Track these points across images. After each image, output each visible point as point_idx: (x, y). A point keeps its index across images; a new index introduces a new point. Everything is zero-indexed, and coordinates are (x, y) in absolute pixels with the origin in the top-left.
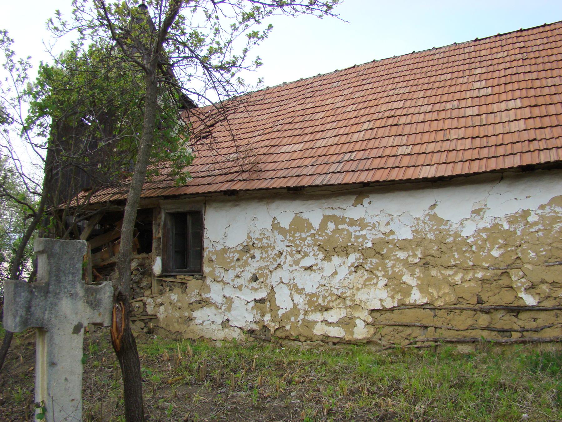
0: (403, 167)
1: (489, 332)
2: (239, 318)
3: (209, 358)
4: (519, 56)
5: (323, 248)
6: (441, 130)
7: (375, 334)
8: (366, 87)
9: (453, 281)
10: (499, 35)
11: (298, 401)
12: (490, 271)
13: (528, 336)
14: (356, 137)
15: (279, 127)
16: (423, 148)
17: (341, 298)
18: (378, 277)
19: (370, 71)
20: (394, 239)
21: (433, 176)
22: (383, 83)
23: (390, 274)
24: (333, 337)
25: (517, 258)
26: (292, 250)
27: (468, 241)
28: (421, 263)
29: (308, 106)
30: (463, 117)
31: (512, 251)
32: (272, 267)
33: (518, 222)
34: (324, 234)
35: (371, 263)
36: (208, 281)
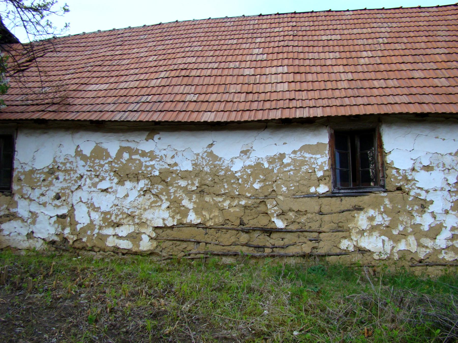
0: (189, 111)
1: (248, 247)
2: (43, 231)
3: (12, 265)
4: (291, 33)
5: (117, 174)
6: (223, 84)
7: (157, 247)
8: (167, 42)
9: (222, 206)
10: (278, 14)
11: (86, 301)
12: (252, 200)
13: (277, 251)
14: (153, 83)
15: (90, 69)
16: (207, 98)
17: (131, 216)
18: (162, 200)
19: (172, 29)
20: (177, 170)
21: (212, 121)
22: (182, 40)
23: (172, 198)
24: (122, 249)
25: (273, 191)
26: (91, 175)
27: (236, 175)
28: (198, 191)
29: (117, 53)
30: (242, 75)
31: (269, 185)
32: (73, 188)
33: (275, 162)
34: (119, 162)
35: (157, 188)
36: (16, 198)
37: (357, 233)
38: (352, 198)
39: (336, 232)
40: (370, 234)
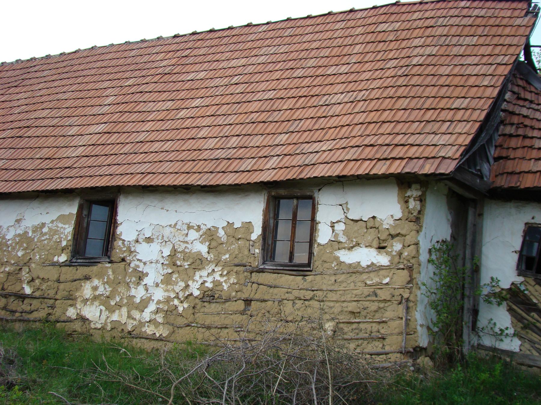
13: (26, 316)
37: (82, 301)
38: (86, 267)
39: (67, 299)
40: (92, 304)
